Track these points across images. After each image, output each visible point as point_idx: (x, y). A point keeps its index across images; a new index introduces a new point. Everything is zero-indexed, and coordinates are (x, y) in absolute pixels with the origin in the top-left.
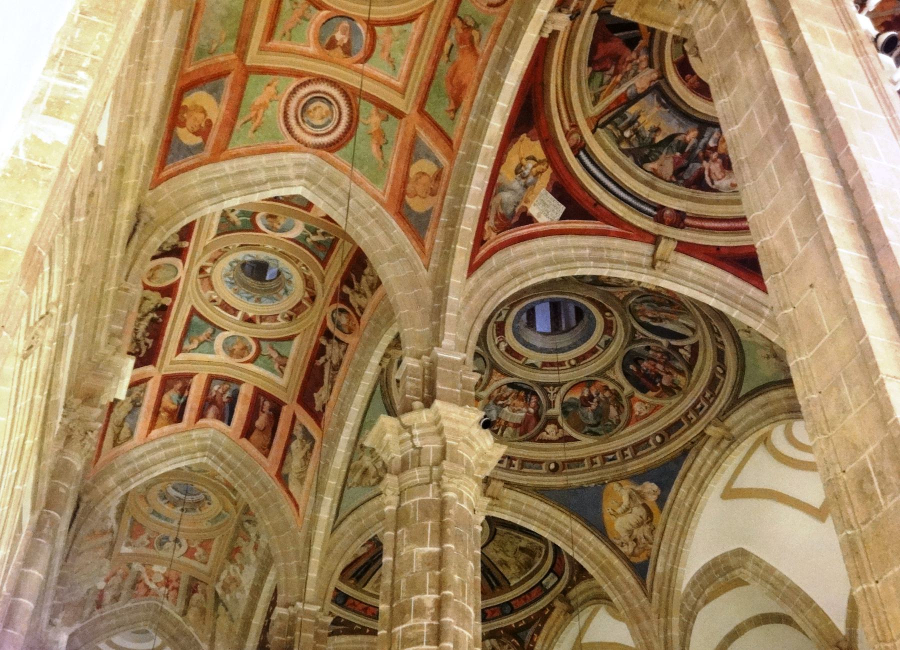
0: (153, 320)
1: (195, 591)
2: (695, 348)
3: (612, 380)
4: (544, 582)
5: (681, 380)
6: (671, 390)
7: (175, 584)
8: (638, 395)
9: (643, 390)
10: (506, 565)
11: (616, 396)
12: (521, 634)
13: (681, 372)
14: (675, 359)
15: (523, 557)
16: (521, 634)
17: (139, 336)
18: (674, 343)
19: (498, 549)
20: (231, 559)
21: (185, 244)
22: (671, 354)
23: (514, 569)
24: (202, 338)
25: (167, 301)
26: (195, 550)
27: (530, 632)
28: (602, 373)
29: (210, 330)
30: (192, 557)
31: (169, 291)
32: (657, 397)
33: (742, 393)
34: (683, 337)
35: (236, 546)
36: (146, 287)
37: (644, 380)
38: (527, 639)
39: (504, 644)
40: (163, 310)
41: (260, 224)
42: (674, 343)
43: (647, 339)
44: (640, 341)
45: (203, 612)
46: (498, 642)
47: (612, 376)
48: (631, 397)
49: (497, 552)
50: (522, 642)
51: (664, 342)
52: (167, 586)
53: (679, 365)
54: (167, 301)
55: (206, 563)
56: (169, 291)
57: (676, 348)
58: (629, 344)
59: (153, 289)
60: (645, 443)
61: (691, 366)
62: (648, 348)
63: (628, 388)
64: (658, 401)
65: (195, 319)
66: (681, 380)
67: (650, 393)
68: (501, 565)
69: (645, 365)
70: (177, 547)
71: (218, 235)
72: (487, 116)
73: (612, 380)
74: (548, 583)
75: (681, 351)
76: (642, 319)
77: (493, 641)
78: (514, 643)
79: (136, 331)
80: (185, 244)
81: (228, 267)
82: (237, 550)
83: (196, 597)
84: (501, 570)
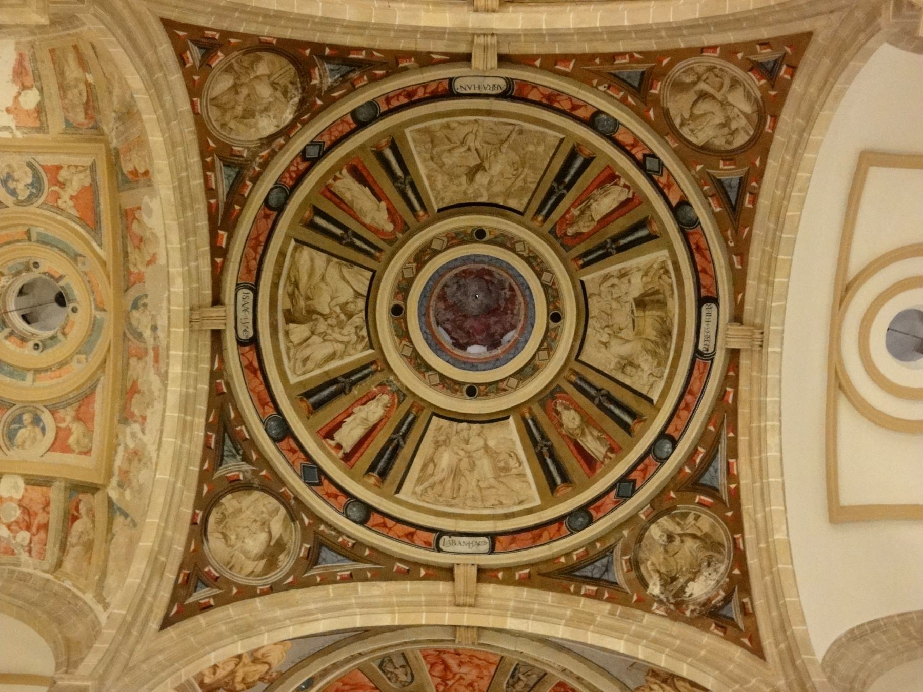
1: (75, 518)
4: (701, 347)
7: (40, 519)
10: (631, 364)
12: (706, 479)
15: (649, 320)
16: (706, 479)
19: (605, 338)
20: (126, 418)
23: (646, 364)
26: (69, 431)
27: (720, 463)
30: (66, 449)
35: (129, 385)
38: (721, 481)
39: (685, 515)
45: (89, 546)
46: (673, 517)
49: (606, 345)
50: (712, 491)
52: (28, 528)
55: (87, 452)
68: (623, 368)
70: (39, 436)
72: (444, 33)
74: (709, 314)
77: (664, 521)
78: (701, 504)
82: (133, 390)
83: (78, 526)
84: (627, 382)
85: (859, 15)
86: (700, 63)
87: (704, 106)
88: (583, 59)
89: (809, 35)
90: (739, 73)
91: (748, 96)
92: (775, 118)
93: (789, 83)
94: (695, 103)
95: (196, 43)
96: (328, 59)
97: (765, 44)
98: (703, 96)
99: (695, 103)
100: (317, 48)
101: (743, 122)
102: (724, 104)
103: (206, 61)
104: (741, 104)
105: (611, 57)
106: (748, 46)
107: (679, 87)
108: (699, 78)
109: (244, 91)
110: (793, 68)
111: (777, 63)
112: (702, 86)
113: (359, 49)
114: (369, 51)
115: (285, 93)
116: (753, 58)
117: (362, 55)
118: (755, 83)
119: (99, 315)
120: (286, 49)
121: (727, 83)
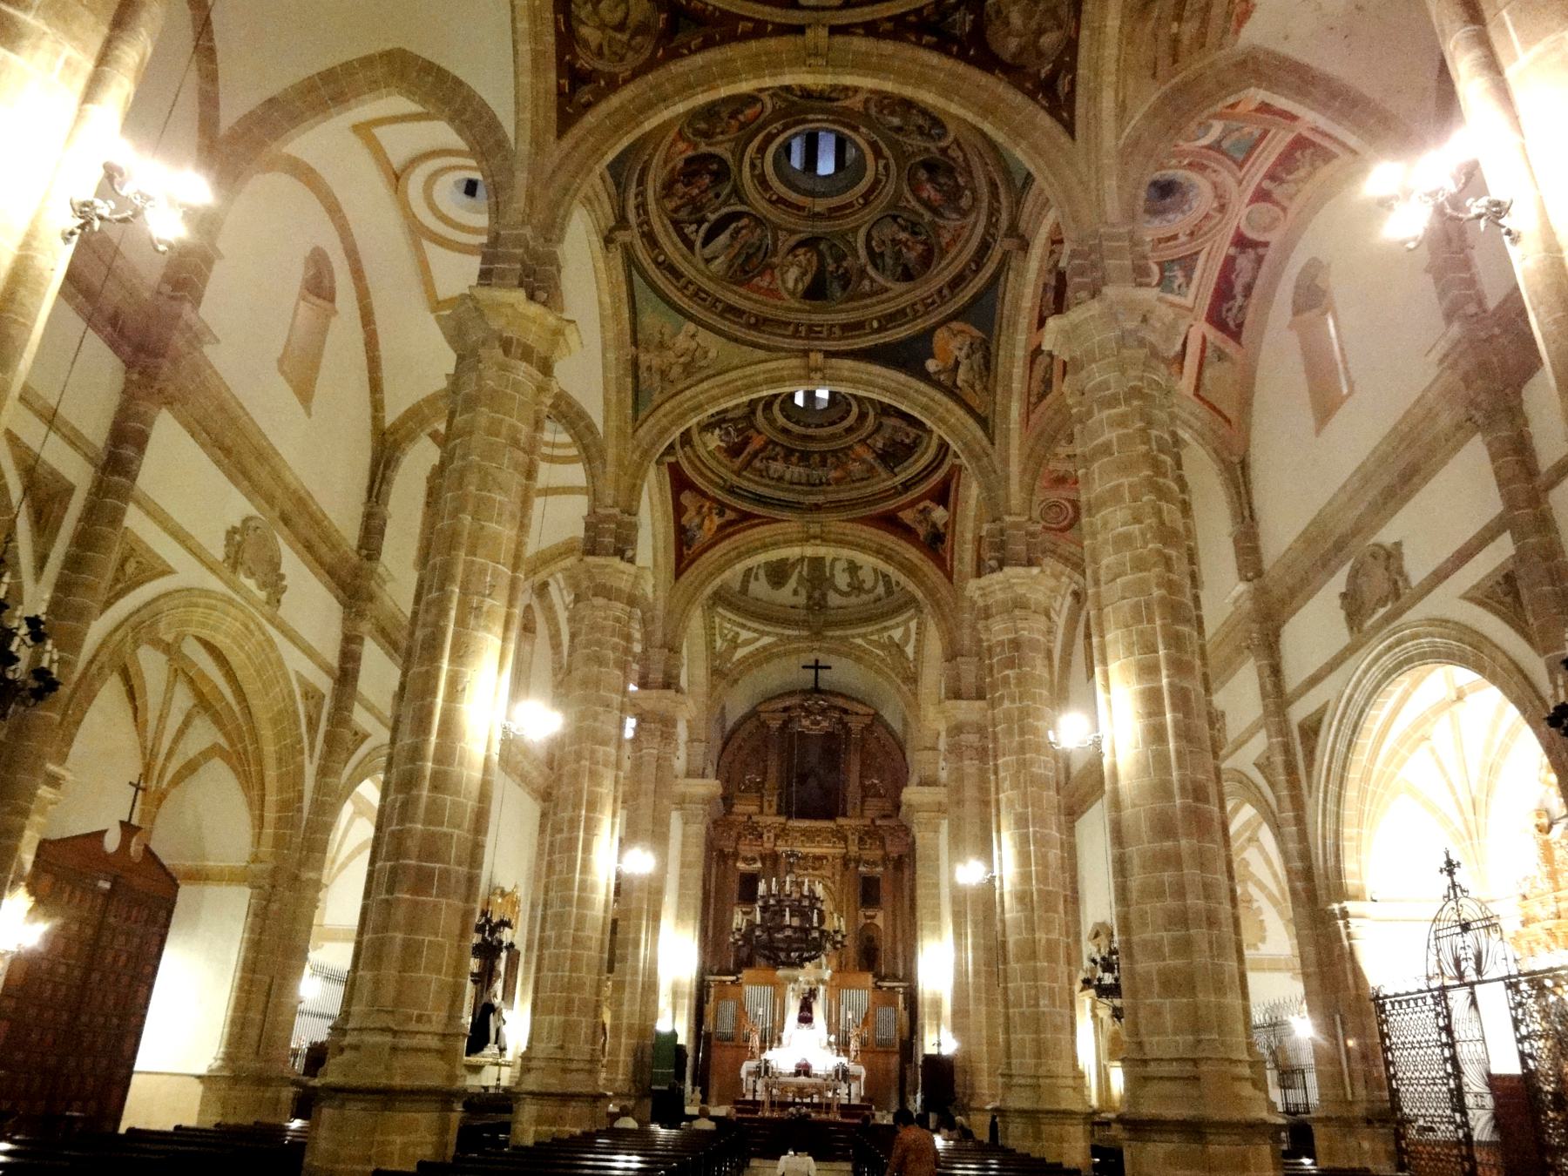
0: (1289, 172)
2: (690, 245)
3: (722, 142)
5: (670, 205)
6: (668, 188)
8: (690, 153)
9: (688, 161)
11: (707, 135)
13: (676, 210)
14: (691, 213)
17: (1308, 168)
18: (705, 226)
21: (1232, 251)
22: (697, 209)
24: (1237, 134)
25: (1267, 184)
28: (777, 228)
29: (1225, 144)
31: (1262, 196)
32: (673, 169)
33: (634, 272)
34: (705, 243)
36: (1284, 209)
37: (694, 167)
40: (1272, 176)
41: (1155, 269)
42: (705, 226)
43: (725, 203)
44: (729, 196)
47: (727, 145)
48: (696, 146)
51: (712, 217)
53: (683, 214)
54: (1267, 184)
56: (1262, 196)
57: (700, 222)
58: (735, 186)
59: (1276, 203)
60: (738, 312)
61: (677, 224)
62: (717, 196)
63: (704, 148)
64: (670, 166)
65: (1240, 157)
66: (670, 205)
67: (681, 164)
69: (707, 180)
71: (1197, 253)
73: (722, 142)
75: (694, 227)
76: (745, 221)
79: (1310, 174)
80: (1232, 251)
81: (1195, 205)
85: (1108, 979)
86: (632, 61)
87: (619, 15)
88: (732, 37)
89: (560, 134)
90: (600, 65)
91: (586, 44)
92: (558, 33)
93: (559, 76)
94: (627, 14)
95: (1057, 97)
96: (955, 40)
97: (588, 106)
98: (621, 27)
99: (627, 14)
100: (962, 56)
101: (583, 15)
102: (602, 26)
103: (1053, 77)
104: (588, 32)
105: (707, 44)
106: (601, 96)
107: (643, 29)
108: (629, 44)
109: (1033, 25)
110: (560, 93)
111: (573, 89)
112: (624, 37)
113: (929, 47)
114: (919, 44)
115: (999, 12)
116: (591, 87)
117: (927, 39)
118: (585, 62)
119: (1183, 238)
120: (988, 61)
121: (606, 50)
